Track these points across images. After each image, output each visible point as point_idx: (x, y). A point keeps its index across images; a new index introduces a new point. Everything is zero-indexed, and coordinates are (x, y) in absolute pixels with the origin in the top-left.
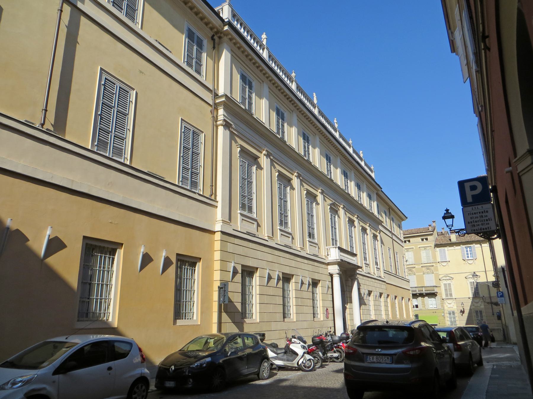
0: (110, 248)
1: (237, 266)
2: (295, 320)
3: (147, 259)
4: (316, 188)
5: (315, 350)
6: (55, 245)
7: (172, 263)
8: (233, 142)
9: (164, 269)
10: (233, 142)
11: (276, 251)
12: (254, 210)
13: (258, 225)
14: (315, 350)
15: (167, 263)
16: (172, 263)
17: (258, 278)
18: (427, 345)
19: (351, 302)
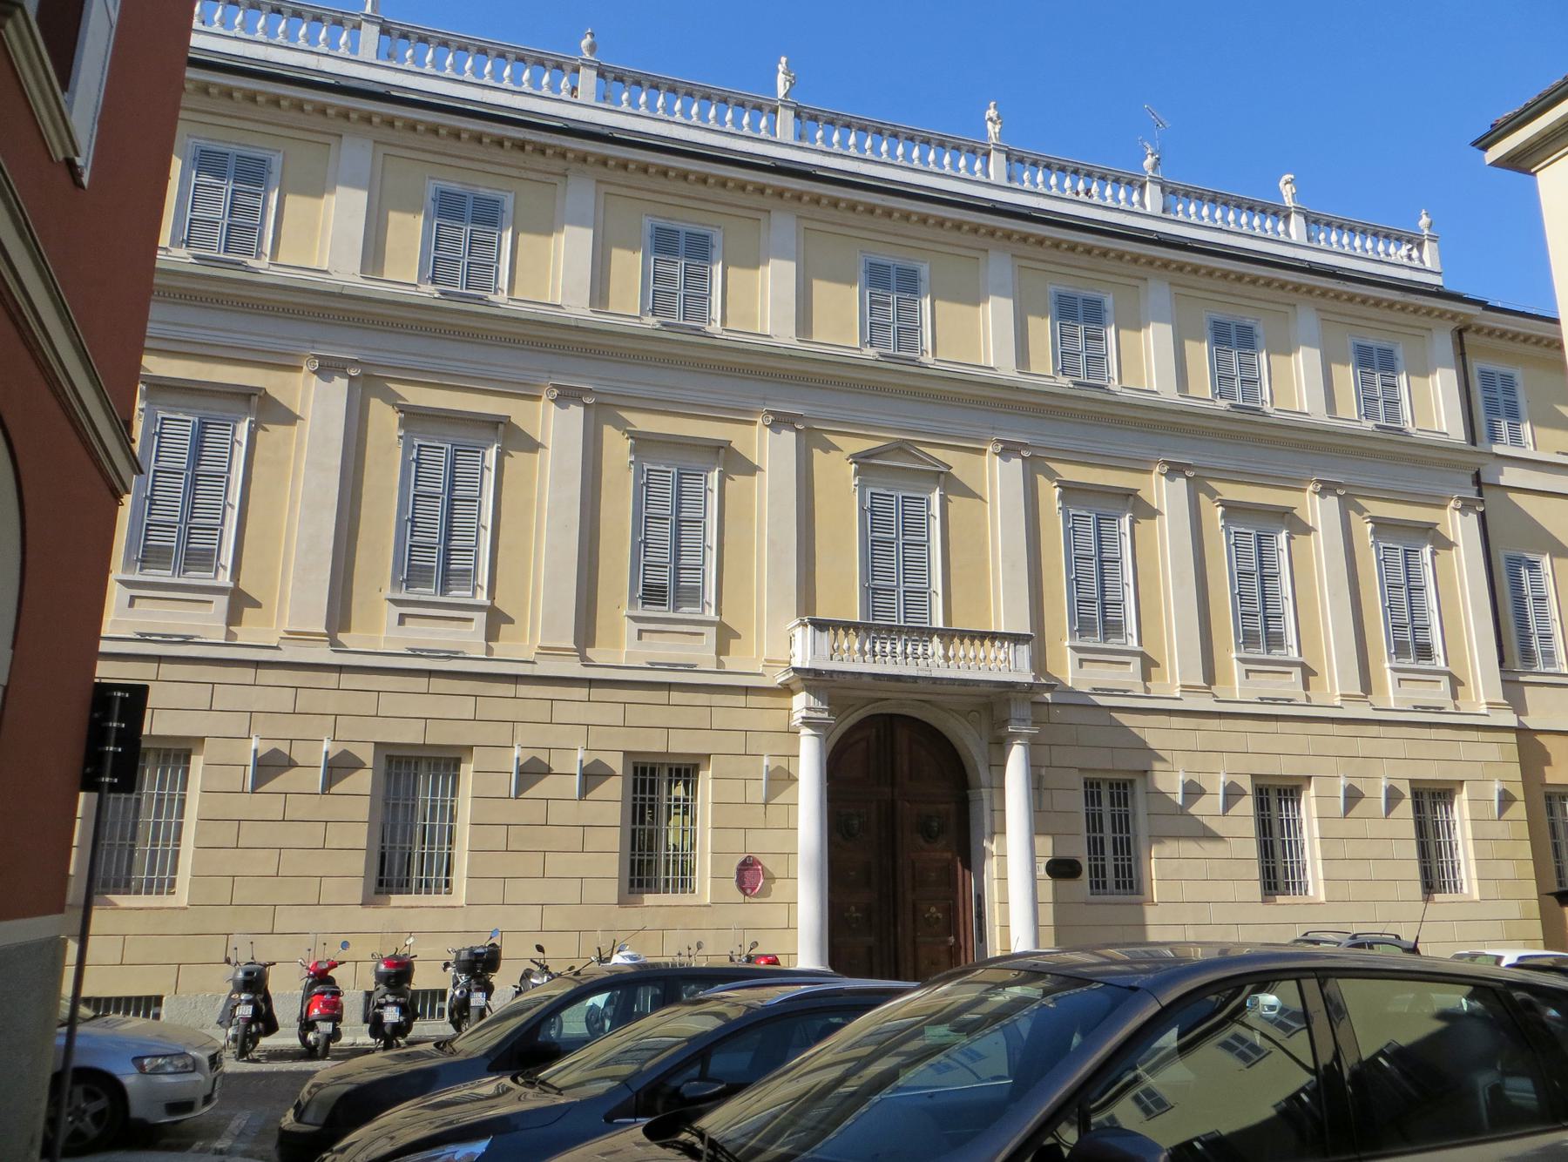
0: (447, 762)
1: (1397, 784)
2: (1322, 898)
3: (1353, 796)
4: (740, 415)
5: (453, 1039)
6: (1193, 791)
7: (1401, 797)
8: (1203, 497)
9: (1389, 808)
10: (1203, 497)
11: (1174, 719)
12: (1438, 648)
13: (1456, 682)
14: (453, 1039)
15: (1393, 797)
16: (1401, 797)
17: (1313, 801)
18: (1482, 1103)
19: (1004, 833)
